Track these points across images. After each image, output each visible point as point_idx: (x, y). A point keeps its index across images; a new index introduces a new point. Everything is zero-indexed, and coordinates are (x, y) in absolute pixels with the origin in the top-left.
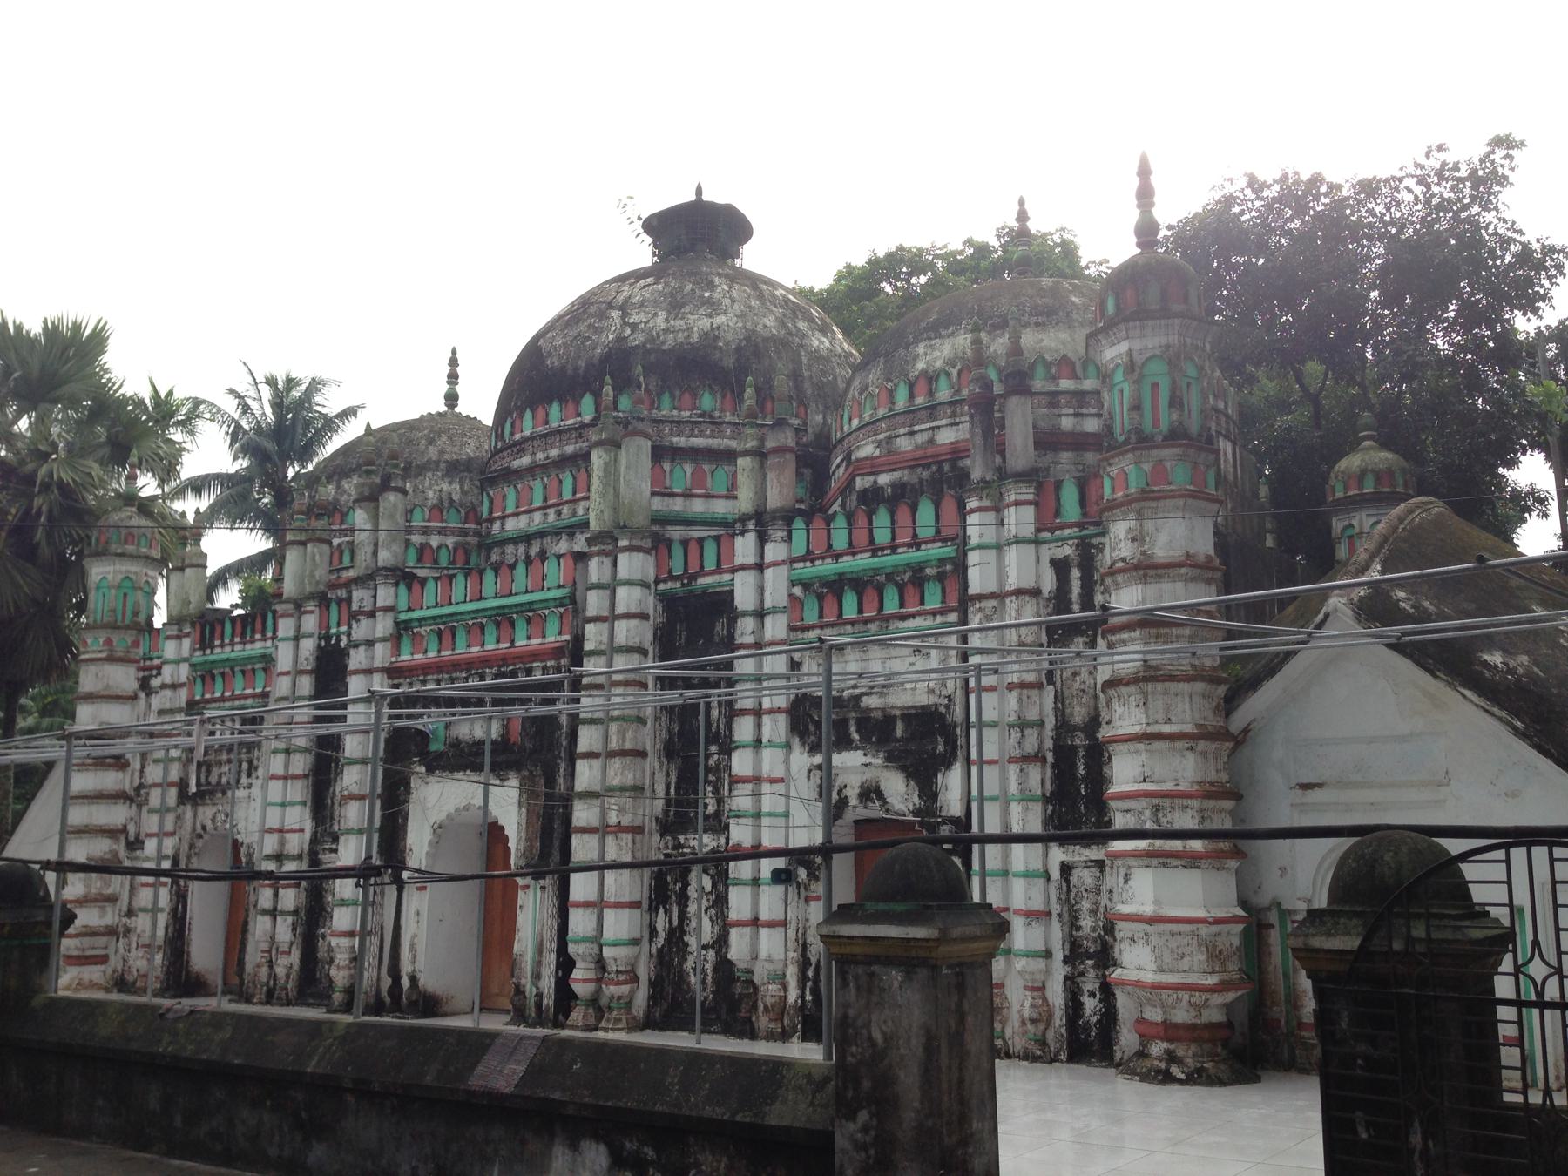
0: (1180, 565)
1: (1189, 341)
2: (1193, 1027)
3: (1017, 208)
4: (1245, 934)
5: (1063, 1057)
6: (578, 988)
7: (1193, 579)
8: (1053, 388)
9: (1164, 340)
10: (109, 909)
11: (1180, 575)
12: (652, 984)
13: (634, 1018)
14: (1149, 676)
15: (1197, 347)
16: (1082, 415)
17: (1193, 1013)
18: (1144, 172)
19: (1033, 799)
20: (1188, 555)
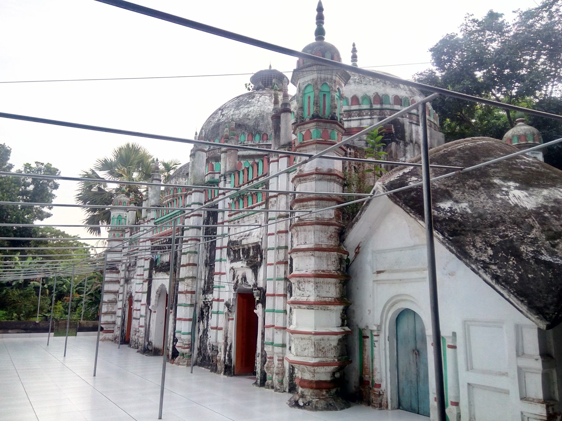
0: (312, 174)
2: (311, 382)
3: (352, 47)
4: (340, 340)
5: (287, 390)
6: (179, 349)
7: (320, 180)
10: (114, 316)
11: (313, 179)
16: (350, 120)
17: (312, 375)
18: (320, 9)
19: (279, 279)
20: (317, 169)
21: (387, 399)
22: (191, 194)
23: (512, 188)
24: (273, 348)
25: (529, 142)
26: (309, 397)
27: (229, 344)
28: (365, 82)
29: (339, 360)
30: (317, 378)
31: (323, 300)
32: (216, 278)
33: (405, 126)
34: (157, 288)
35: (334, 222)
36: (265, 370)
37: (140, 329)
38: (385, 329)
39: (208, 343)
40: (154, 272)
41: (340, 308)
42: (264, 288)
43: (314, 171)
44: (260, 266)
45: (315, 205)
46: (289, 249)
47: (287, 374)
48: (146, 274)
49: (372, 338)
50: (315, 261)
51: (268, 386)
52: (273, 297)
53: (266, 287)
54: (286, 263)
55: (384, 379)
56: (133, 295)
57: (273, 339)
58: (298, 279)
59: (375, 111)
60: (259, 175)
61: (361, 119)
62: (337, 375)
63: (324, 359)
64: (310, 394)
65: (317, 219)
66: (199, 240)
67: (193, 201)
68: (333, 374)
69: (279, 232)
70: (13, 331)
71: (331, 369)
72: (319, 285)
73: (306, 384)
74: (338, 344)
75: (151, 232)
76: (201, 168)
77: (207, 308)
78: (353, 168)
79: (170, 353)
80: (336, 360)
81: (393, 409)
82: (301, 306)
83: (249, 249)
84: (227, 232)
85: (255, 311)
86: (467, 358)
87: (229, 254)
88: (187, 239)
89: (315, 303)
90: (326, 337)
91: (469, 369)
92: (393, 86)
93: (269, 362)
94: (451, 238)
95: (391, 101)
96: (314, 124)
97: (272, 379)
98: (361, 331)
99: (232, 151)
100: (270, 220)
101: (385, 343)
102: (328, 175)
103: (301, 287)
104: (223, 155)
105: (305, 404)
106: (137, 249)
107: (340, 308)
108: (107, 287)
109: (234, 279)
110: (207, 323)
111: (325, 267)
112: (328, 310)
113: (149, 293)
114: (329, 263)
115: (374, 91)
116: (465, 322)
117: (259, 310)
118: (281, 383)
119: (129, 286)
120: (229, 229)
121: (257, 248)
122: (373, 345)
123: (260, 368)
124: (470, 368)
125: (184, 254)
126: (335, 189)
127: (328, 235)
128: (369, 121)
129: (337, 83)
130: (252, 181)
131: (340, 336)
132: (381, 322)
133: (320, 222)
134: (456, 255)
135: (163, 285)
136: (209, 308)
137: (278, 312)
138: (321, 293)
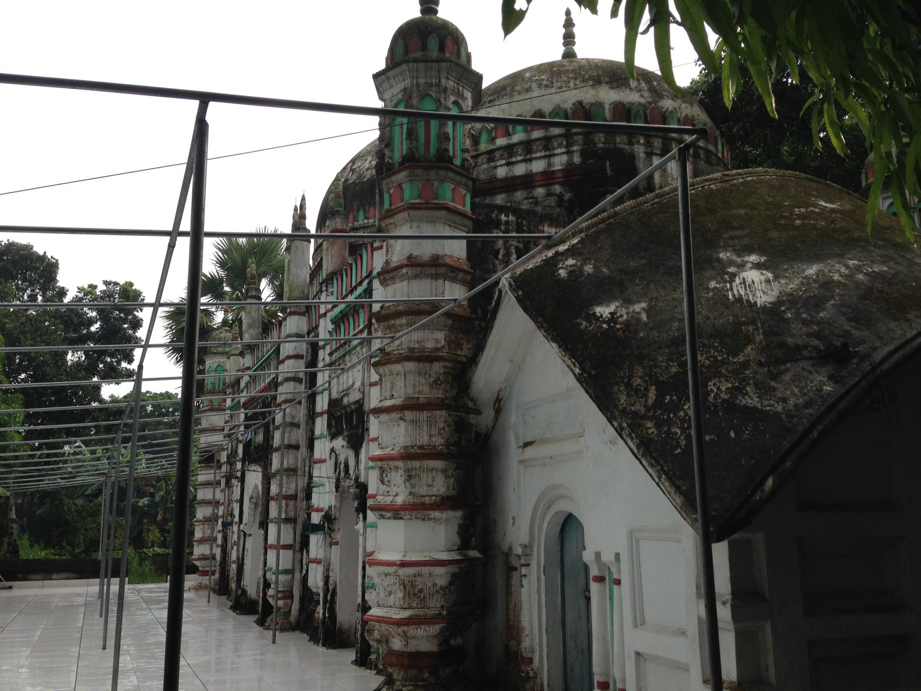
0: (401, 267)
1: (422, 81)
4: (454, 577)
7: (416, 277)
8: (492, 147)
9: (402, 86)
11: (404, 275)
13: (290, 623)
15: (431, 85)
20: (410, 257)
21: (542, 685)
26: (398, 683)
27: (331, 588)
28: (559, 84)
29: (449, 613)
30: (413, 647)
31: (418, 500)
33: (637, 161)
35: (443, 354)
38: (538, 552)
41: (455, 516)
43: (405, 262)
50: (407, 430)
51: (371, 663)
55: (537, 648)
59: (576, 138)
63: (421, 612)
65: (411, 350)
70: (62, 575)
71: (434, 629)
72: (413, 474)
74: (451, 583)
76: (299, 272)
78: (513, 251)
82: (384, 513)
86: (635, 603)
89: (405, 508)
90: (425, 570)
91: (639, 624)
92: (615, 85)
95: (608, 114)
96: (405, 173)
101: (539, 580)
102: (435, 268)
103: (386, 479)
111: (425, 440)
112: (430, 519)
114: (433, 432)
115: (574, 100)
116: (631, 533)
124: (639, 622)
127: (432, 380)
128: (565, 158)
129: (449, 92)
132: (532, 536)
138: (417, 489)
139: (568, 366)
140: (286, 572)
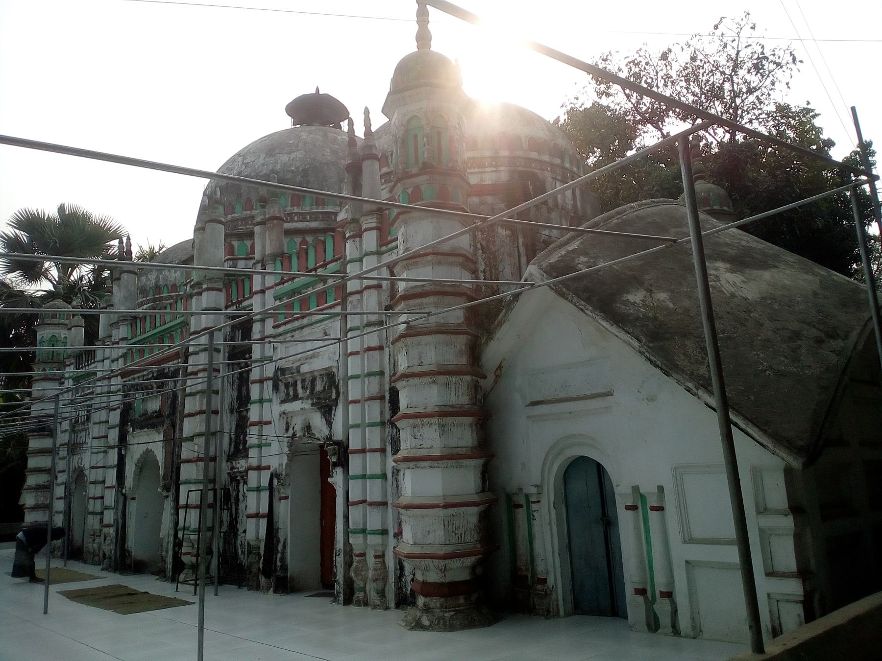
6: (185, 559)
7: (440, 263)
12: (219, 555)
14: (412, 332)
21: (557, 599)
22: (200, 294)
23: (722, 270)
24: (365, 539)
25: (715, 207)
26: (438, 610)
30: (450, 577)
32: (253, 431)
34: (137, 456)
36: (352, 574)
37: (105, 530)
39: (239, 542)
40: (131, 429)
42: (345, 441)
44: (336, 405)
45: (434, 303)
46: (387, 375)
47: (392, 579)
48: (114, 436)
49: (528, 507)
52: (361, 455)
53: (348, 439)
54: (382, 398)
55: (551, 569)
56: (86, 472)
57: (365, 523)
58: (411, 421)
60: (329, 259)
61: (481, 173)
62: (479, 571)
64: (438, 605)
66: (218, 371)
67: (204, 306)
68: (473, 568)
69: (370, 349)
71: (469, 561)
73: (429, 589)
75: (121, 361)
77: (235, 483)
79: (169, 566)
80: (479, 546)
81: (567, 614)
83: (313, 381)
84: (270, 354)
85: (330, 480)
87: (276, 388)
88: (195, 369)
93: (358, 561)
94: (651, 345)
97: (364, 589)
98: (509, 497)
99: (275, 222)
100: (351, 330)
104: (257, 229)
105: (432, 623)
106: (92, 393)
107: (480, 462)
108: (32, 462)
109: (287, 430)
110: (237, 509)
111: (454, 400)
112: (462, 467)
113: (121, 466)
117: (337, 478)
118: (382, 594)
119: (76, 458)
120: (275, 348)
121: (330, 377)
122: (530, 518)
123: (342, 573)
125: (191, 394)
126: (464, 278)
130: (315, 269)
131: (482, 508)
133: (442, 330)
134: (662, 369)
135: (148, 452)
136: (238, 483)
137: (373, 477)
139: (625, 342)
140: (209, 529)
